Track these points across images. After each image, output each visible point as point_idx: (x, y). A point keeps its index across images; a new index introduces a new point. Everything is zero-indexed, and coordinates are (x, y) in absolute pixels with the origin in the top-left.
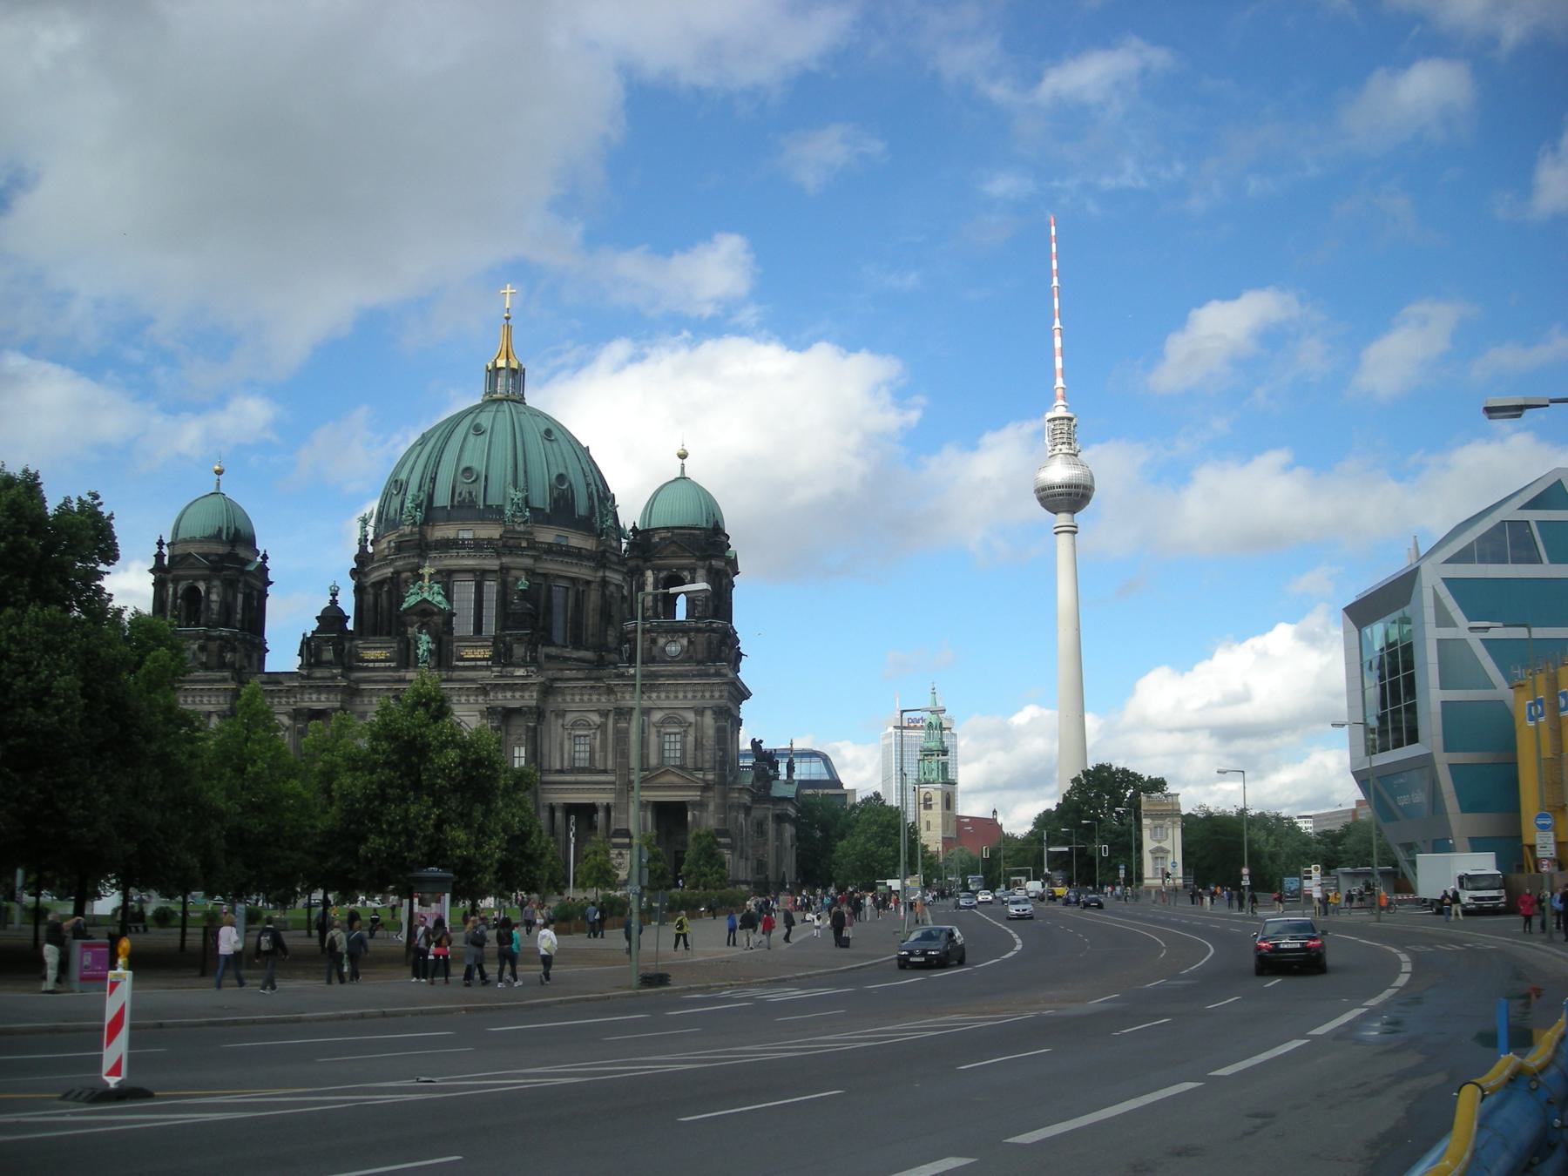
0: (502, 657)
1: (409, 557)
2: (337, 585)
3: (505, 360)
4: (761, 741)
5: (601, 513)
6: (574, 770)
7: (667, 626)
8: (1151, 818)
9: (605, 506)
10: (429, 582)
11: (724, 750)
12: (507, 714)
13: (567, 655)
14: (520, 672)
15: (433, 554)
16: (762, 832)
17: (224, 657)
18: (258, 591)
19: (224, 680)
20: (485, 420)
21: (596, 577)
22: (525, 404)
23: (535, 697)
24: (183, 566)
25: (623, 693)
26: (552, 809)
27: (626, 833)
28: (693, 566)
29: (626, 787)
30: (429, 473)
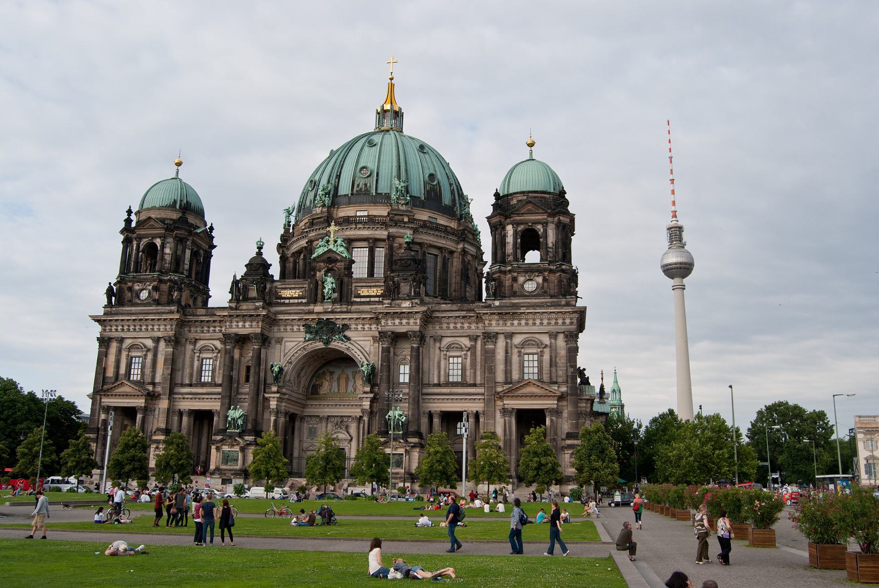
0: (392, 292)
1: (320, 229)
3: (390, 105)
4: (584, 369)
5: (460, 204)
6: (448, 384)
12: (397, 338)
14: (406, 304)
17: (172, 296)
18: (204, 250)
19: (171, 312)
20: (377, 139)
26: (431, 416)
30: (336, 172)
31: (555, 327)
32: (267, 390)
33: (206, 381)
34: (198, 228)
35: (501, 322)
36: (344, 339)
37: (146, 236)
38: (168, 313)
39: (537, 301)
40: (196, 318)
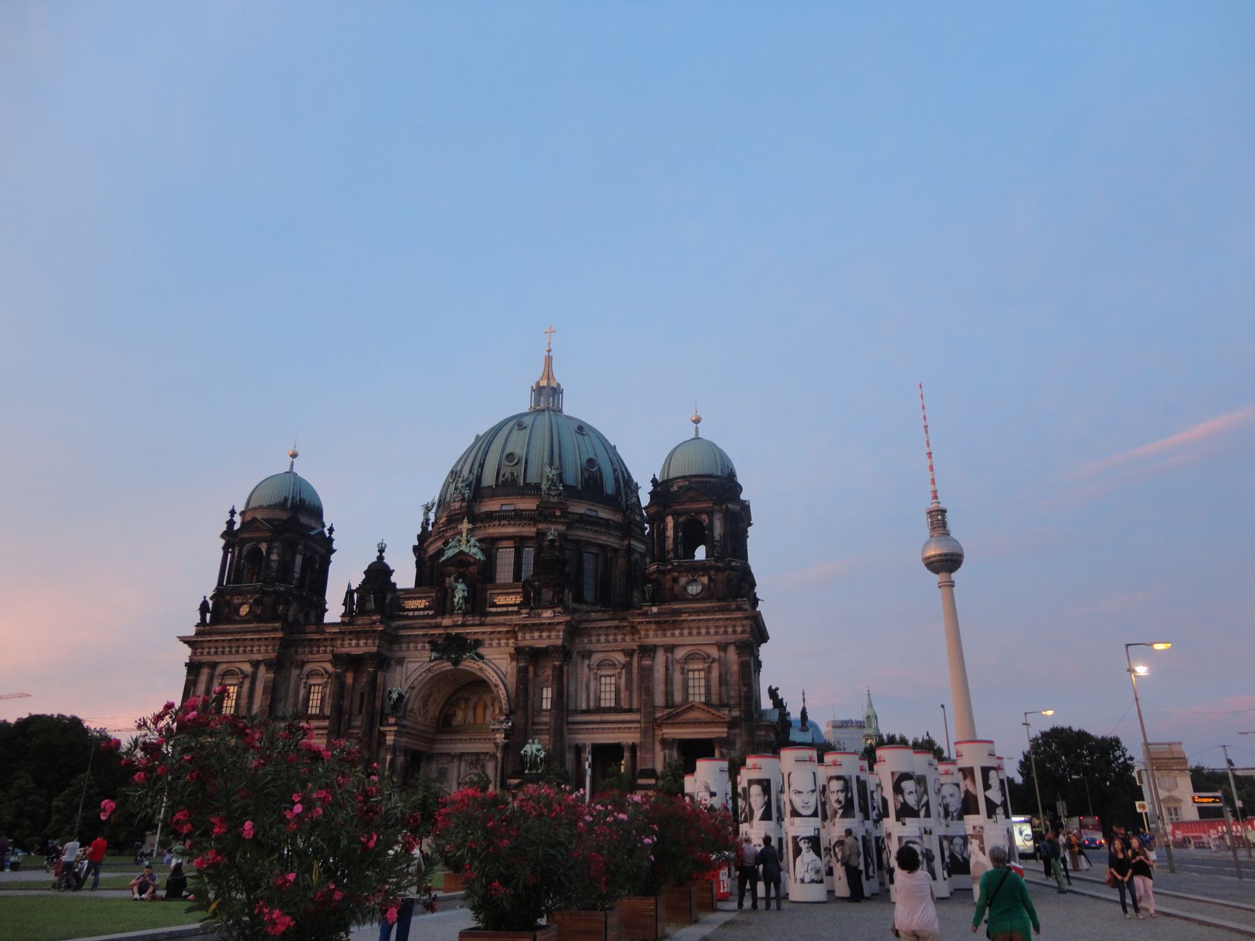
4: (777, 689)
5: (626, 494)
10: (467, 536)
14: (547, 614)
17: (277, 611)
19: (275, 630)
20: (527, 421)
21: (622, 546)
23: (561, 637)
24: (249, 530)
26: (578, 750)
29: (651, 725)
31: (725, 637)
32: (384, 723)
33: (313, 712)
34: (313, 529)
35: (660, 633)
36: (476, 657)
37: (250, 540)
38: (271, 631)
39: (702, 605)
40: (303, 636)
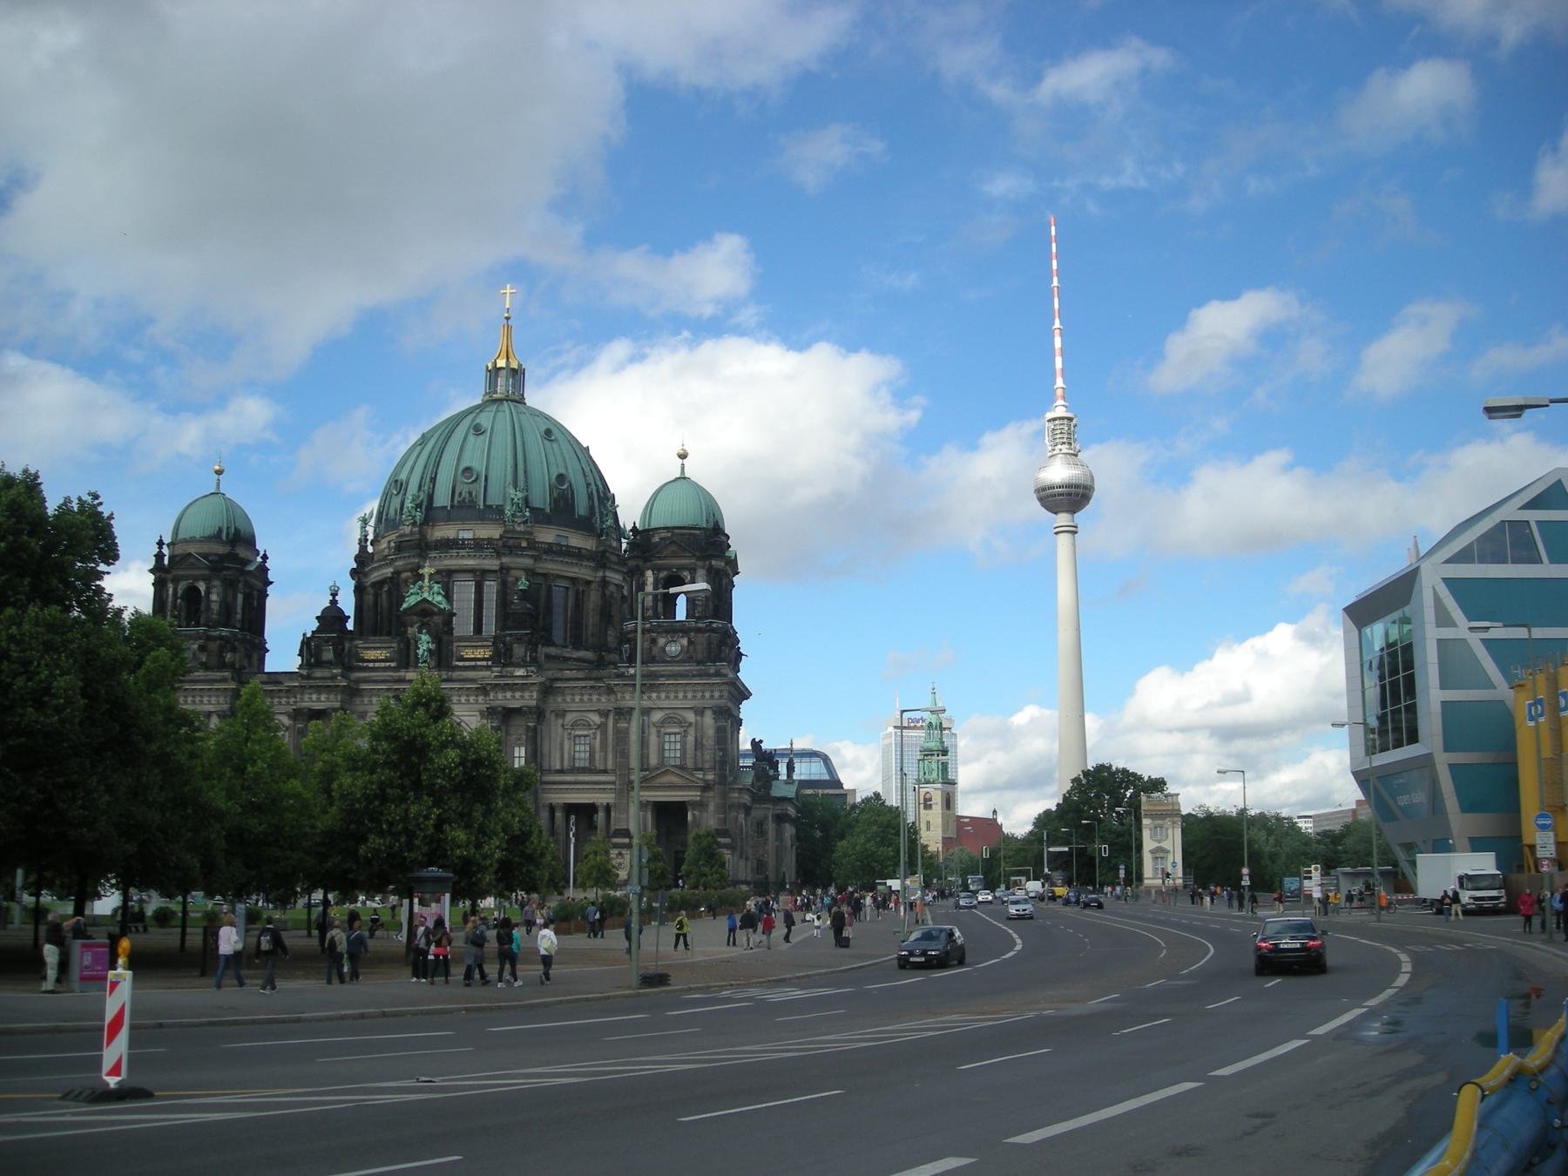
0: (502, 657)
1: (409, 557)
2: (337, 585)
3: (505, 360)
4: (761, 741)
5: (601, 513)
6: (574, 770)
7: (667, 626)
8: (1151, 818)
9: (605, 506)
10: (429, 582)
11: (724, 750)
12: (507, 714)
13: (567, 655)
14: (520, 672)
15: (433, 554)
16: (762, 832)
17: (224, 657)
18: (258, 591)
19: (224, 680)
20: (485, 420)
21: (596, 577)
22: (525, 404)
23: (535, 697)
24: (183, 566)
25: (623, 693)
26: (552, 809)
27: (626, 833)
28: (693, 566)
29: (626, 787)
30: (429, 473)
